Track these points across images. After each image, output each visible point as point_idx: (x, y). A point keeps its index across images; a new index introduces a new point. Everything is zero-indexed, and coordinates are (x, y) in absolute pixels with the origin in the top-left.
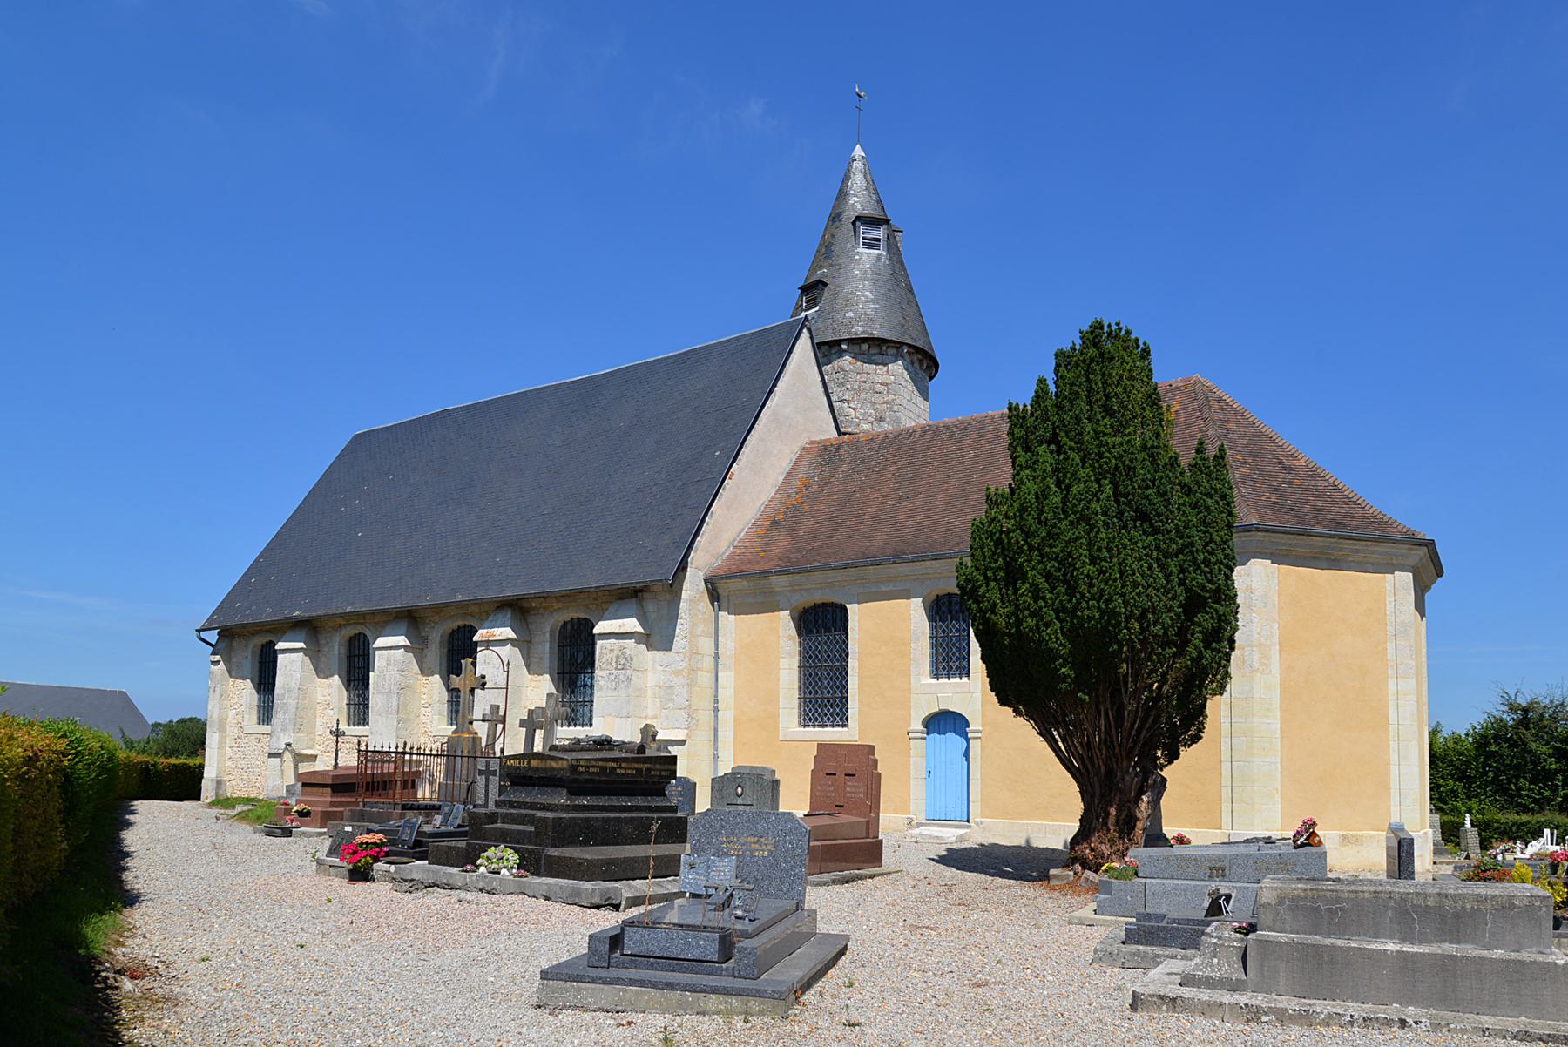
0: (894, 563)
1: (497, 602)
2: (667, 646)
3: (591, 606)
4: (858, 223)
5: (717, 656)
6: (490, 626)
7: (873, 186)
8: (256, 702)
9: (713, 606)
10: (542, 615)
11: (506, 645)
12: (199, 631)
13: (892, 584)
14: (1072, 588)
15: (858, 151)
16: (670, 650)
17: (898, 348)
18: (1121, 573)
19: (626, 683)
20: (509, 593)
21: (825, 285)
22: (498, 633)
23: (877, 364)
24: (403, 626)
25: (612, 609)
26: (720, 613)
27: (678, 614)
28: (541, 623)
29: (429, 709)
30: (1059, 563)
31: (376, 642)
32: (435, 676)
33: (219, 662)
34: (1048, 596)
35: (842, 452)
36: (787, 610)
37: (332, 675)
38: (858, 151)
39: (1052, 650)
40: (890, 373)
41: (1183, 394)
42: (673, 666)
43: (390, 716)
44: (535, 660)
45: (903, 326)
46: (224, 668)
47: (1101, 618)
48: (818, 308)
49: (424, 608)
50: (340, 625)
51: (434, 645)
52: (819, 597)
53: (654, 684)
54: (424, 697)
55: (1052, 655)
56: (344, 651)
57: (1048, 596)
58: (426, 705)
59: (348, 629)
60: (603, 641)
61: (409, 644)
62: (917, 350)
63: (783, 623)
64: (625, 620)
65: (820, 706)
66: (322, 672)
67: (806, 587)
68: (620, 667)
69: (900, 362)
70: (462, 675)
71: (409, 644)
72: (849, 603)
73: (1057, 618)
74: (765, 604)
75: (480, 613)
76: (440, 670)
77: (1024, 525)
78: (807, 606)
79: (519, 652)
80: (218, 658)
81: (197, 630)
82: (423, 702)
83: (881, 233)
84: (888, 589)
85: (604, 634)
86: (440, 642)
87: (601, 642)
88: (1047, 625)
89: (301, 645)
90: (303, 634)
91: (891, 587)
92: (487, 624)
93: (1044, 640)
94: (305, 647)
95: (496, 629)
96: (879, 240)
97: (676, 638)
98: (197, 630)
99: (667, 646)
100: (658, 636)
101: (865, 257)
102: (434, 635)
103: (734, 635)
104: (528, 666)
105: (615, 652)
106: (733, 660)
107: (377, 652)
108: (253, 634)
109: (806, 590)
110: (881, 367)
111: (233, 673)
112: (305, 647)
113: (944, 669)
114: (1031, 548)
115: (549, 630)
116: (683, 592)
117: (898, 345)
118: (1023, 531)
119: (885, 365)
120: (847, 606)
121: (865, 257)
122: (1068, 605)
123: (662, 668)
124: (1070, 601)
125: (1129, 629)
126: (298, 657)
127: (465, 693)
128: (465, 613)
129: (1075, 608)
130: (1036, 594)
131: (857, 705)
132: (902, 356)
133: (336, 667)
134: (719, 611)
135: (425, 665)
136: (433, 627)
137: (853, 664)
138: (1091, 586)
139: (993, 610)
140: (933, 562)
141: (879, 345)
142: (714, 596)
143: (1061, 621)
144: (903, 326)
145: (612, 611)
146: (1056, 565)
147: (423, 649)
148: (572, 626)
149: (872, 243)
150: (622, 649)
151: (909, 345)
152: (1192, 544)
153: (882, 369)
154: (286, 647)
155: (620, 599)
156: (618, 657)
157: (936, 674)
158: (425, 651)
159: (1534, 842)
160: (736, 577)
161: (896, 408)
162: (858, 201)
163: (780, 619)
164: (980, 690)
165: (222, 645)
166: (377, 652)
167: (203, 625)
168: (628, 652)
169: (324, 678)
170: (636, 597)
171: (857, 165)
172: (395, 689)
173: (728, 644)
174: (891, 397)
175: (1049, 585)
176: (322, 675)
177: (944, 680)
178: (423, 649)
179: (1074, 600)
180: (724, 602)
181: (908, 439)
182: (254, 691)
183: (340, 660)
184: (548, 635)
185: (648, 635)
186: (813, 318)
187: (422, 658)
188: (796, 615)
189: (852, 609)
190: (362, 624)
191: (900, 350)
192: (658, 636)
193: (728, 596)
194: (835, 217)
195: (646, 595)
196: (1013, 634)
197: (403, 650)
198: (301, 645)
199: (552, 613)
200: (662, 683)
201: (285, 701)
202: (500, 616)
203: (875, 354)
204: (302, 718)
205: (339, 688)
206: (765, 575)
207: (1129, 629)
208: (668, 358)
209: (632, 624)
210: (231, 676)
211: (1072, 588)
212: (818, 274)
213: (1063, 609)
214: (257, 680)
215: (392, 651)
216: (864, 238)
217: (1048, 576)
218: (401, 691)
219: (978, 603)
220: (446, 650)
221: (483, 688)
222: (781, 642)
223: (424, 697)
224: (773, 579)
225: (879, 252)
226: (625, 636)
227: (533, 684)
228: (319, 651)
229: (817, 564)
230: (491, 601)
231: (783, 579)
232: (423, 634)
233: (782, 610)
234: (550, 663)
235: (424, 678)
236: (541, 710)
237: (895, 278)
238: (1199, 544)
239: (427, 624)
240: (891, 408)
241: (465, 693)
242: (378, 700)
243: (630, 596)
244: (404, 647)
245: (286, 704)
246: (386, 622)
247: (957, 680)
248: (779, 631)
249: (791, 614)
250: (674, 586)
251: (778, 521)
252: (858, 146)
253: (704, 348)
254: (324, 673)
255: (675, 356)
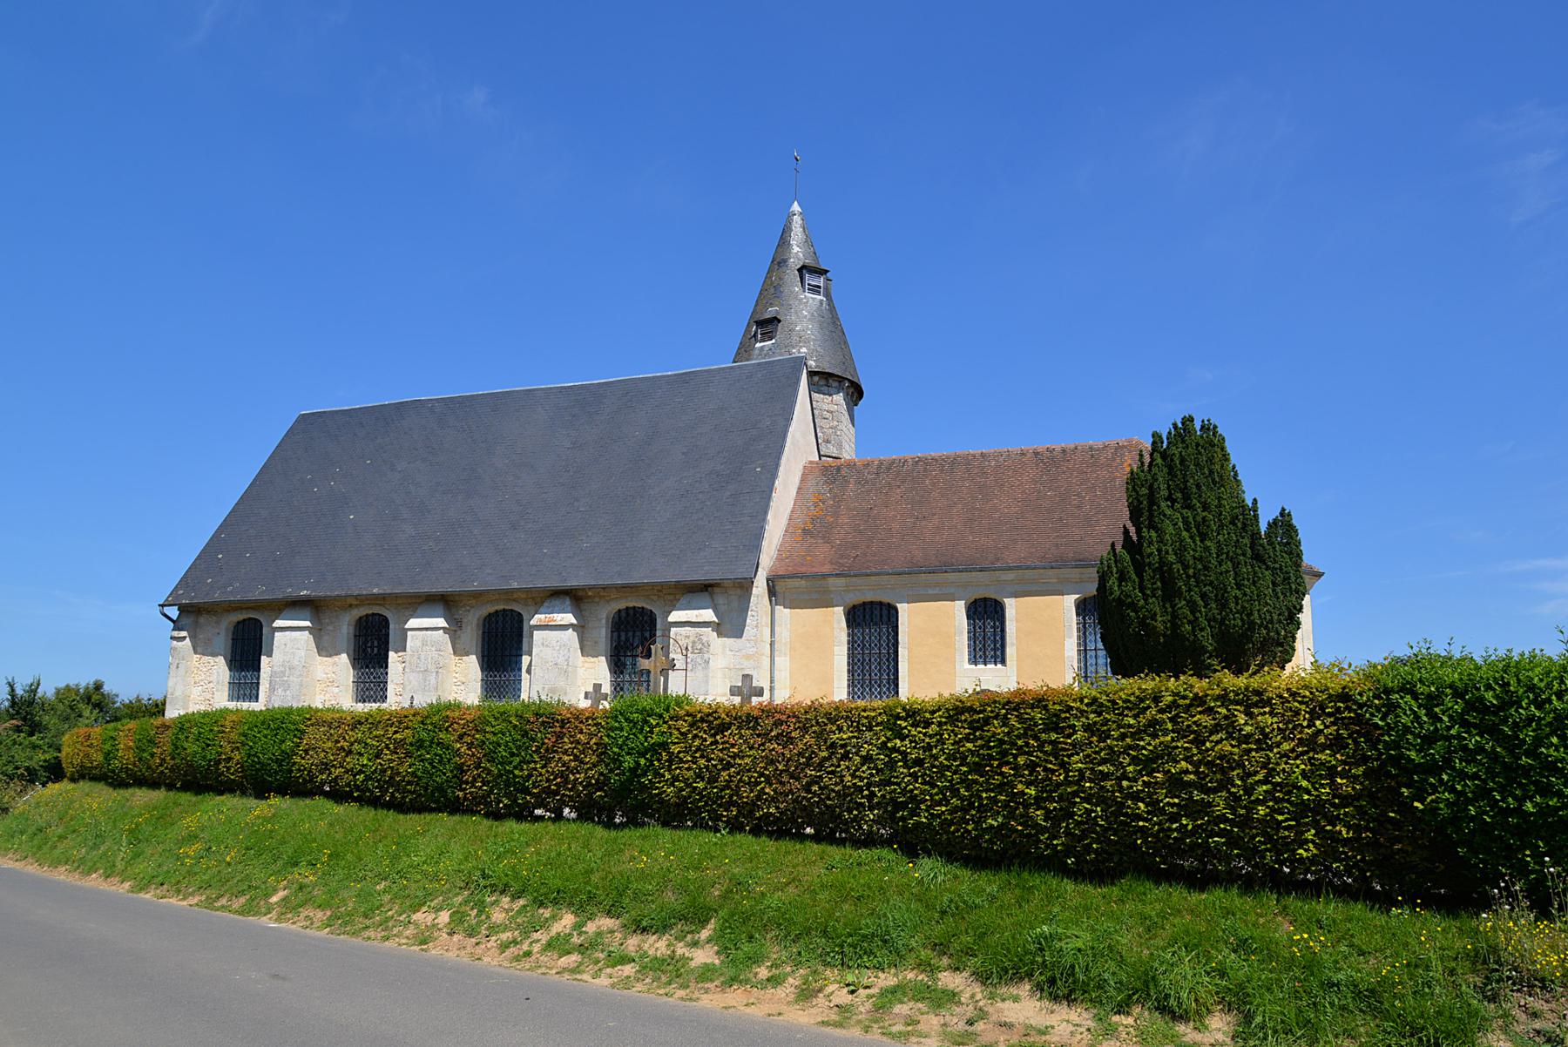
0: (946, 572)
1: (548, 590)
2: (738, 632)
3: (652, 597)
4: (804, 271)
5: (772, 644)
6: (546, 611)
7: (808, 241)
8: (227, 679)
9: (771, 601)
10: (598, 603)
11: (568, 629)
12: (162, 606)
13: (938, 589)
14: (1223, 605)
15: (796, 207)
16: (741, 637)
17: (840, 382)
18: (1258, 596)
19: (703, 665)
20: (572, 583)
21: (779, 321)
22: (559, 619)
23: (824, 394)
24: (440, 608)
25: (683, 600)
26: (777, 607)
27: (748, 607)
28: (597, 610)
29: (462, 687)
30: (1213, 588)
31: (409, 623)
32: (471, 656)
33: (185, 638)
34: (1203, 610)
35: (843, 473)
36: (841, 606)
37: (338, 654)
38: (796, 207)
39: (1204, 646)
40: (834, 402)
41: (1130, 452)
42: (744, 651)
43: (426, 693)
44: (589, 643)
45: (844, 363)
46: (190, 644)
47: (1243, 625)
48: (773, 341)
49: (460, 594)
50: (351, 606)
51: (469, 628)
52: (870, 597)
53: (723, 666)
54: (457, 675)
55: (1203, 650)
56: (352, 630)
57: (1203, 610)
58: (459, 683)
59: (361, 609)
60: (677, 629)
61: (447, 626)
62: (851, 382)
63: (836, 618)
64: (701, 611)
65: (867, 686)
66: (324, 649)
67: (859, 588)
68: (696, 651)
69: (841, 394)
70: (653, 658)
71: (447, 626)
72: (899, 603)
73: (1209, 625)
74: (821, 600)
75: (526, 599)
76: (477, 650)
77: (1185, 560)
78: (855, 603)
79: (312, 639)
80: (184, 634)
81: (159, 605)
82: (456, 680)
83: (821, 282)
84: (935, 592)
85: (682, 622)
86: (478, 625)
87: (675, 629)
88: (1202, 630)
89: (308, 624)
90: (307, 612)
91: (937, 591)
92: (542, 609)
93: (1199, 639)
94: (310, 625)
95: (555, 615)
96: (819, 287)
97: (747, 628)
98: (159, 605)
99: (738, 632)
100: (733, 625)
101: (811, 301)
102: (470, 618)
103: (789, 626)
104: (581, 649)
105: (691, 638)
106: (789, 646)
107: (409, 633)
108: (228, 611)
109: (859, 590)
110: (827, 397)
111: (199, 650)
112: (310, 625)
113: (981, 657)
114: (1188, 577)
115: (604, 616)
116: (754, 589)
117: (841, 379)
118: (1183, 564)
119: (830, 395)
120: (899, 605)
121: (811, 301)
122: (1219, 617)
123: (732, 653)
124: (1221, 614)
125: (1259, 634)
126: (303, 635)
127: (656, 673)
128: (509, 599)
129: (1223, 619)
130: (1193, 607)
131: (906, 685)
132: (843, 389)
133: (345, 645)
134: (776, 605)
135: (457, 646)
136: (469, 611)
137: (903, 652)
138: (1237, 604)
139: (1153, 617)
140: (978, 573)
141: (826, 378)
142: (772, 592)
143: (1211, 627)
144: (844, 363)
145: (684, 602)
146: (1210, 589)
147: (455, 631)
148: (628, 614)
149: (815, 289)
150: (699, 636)
151: (849, 380)
152: (1289, 578)
153: (828, 399)
154: (296, 626)
155: (690, 592)
156: (694, 642)
157: (974, 660)
158: (459, 632)
159: (703, 931)
160: (798, 577)
161: (839, 433)
162: (797, 252)
163: (834, 613)
164: (1015, 674)
165: (186, 621)
166: (409, 633)
167: (167, 600)
168: (705, 639)
169: (327, 656)
170: (707, 590)
171: (797, 219)
172: (431, 667)
173: (783, 632)
174: (835, 423)
175: (1204, 602)
176: (324, 654)
177: (981, 666)
178: (455, 631)
179: (1224, 613)
180: (780, 597)
181: (903, 467)
182: (227, 668)
183: (348, 641)
184: (604, 621)
185: (583, 627)
186: (770, 349)
187: (455, 638)
188: (847, 610)
189: (903, 609)
190: (380, 605)
191: (842, 384)
192: (733, 625)
193: (784, 592)
194: (779, 262)
195: (717, 590)
196: (1167, 636)
197: (442, 631)
198: (308, 624)
199: (608, 601)
200: (732, 666)
201: (286, 678)
202: (554, 602)
203: (822, 386)
204: (305, 695)
205: (347, 666)
206: (824, 576)
207: (1259, 634)
208: (668, 376)
209: (708, 615)
210: (196, 653)
211: (1223, 605)
212: (771, 311)
213: (1215, 620)
214: (229, 657)
215: (429, 632)
216: (809, 285)
217: (1203, 596)
218: (440, 670)
219: (1136, 612)
220: (481, 632)
221: (673, 670)
222: (835, 633)
223: (457, 675)
224: (831, 580)
225: (821, 297)
226: (701, 625)
227: (586, 665)
228: (321, 629)
229: (874, 570)
230: (544, 590)
231: (841, 581)
232: (456, 617)
233: (837, 606)
234: (606, 646)
235: (457, 658)
236: (736, 689)
237: (827, 315)
238: (1293, 579)
239: (461, 607)
240: (835, 432)
241: (656, 673)
242: (411, 678)
243: (700, 591)
244: (572, 625)
245: (287, 681)
246: (420, 603)
247: (992, 666)
248: (833, 624)
249: (844, 610)
250: (746, 586)
251: (808, 529)
252: (796, 203)
253: (705, 371)
254: (327, 651)
255: (675, 375)
